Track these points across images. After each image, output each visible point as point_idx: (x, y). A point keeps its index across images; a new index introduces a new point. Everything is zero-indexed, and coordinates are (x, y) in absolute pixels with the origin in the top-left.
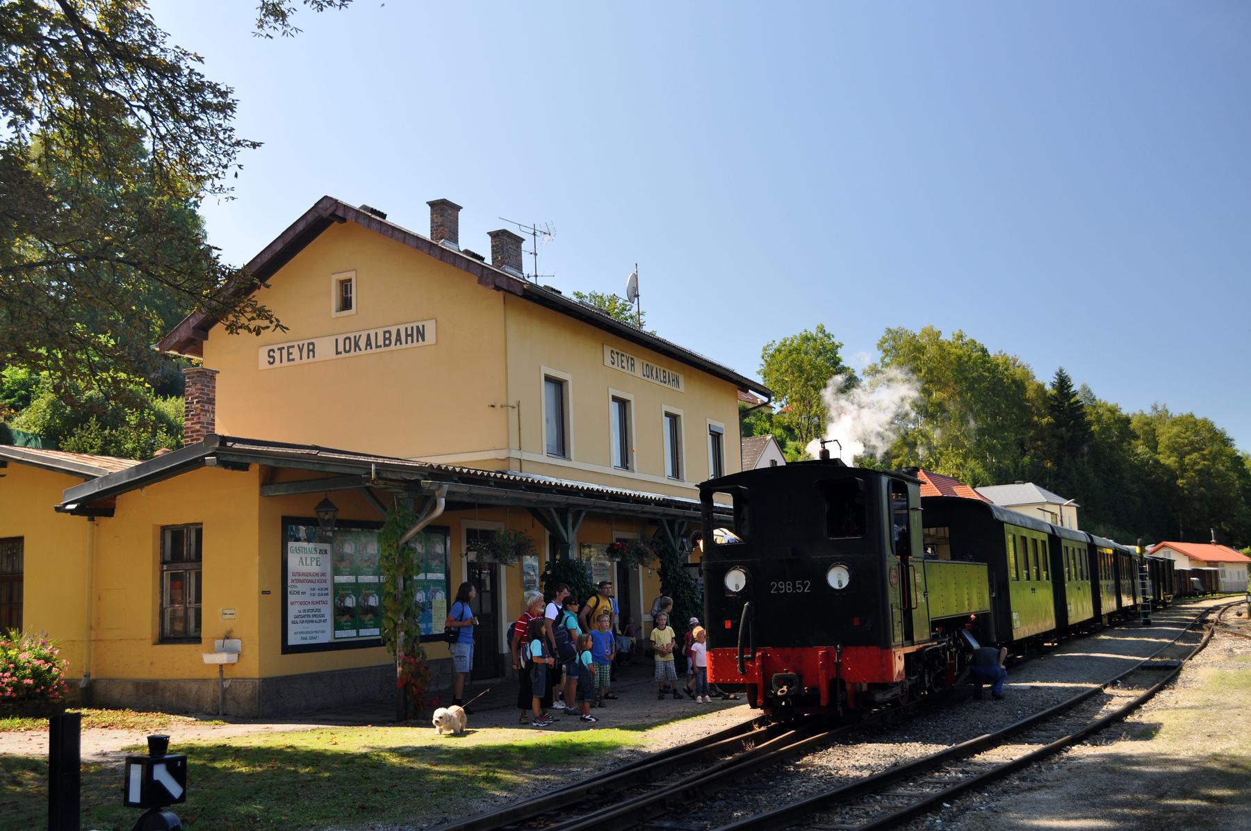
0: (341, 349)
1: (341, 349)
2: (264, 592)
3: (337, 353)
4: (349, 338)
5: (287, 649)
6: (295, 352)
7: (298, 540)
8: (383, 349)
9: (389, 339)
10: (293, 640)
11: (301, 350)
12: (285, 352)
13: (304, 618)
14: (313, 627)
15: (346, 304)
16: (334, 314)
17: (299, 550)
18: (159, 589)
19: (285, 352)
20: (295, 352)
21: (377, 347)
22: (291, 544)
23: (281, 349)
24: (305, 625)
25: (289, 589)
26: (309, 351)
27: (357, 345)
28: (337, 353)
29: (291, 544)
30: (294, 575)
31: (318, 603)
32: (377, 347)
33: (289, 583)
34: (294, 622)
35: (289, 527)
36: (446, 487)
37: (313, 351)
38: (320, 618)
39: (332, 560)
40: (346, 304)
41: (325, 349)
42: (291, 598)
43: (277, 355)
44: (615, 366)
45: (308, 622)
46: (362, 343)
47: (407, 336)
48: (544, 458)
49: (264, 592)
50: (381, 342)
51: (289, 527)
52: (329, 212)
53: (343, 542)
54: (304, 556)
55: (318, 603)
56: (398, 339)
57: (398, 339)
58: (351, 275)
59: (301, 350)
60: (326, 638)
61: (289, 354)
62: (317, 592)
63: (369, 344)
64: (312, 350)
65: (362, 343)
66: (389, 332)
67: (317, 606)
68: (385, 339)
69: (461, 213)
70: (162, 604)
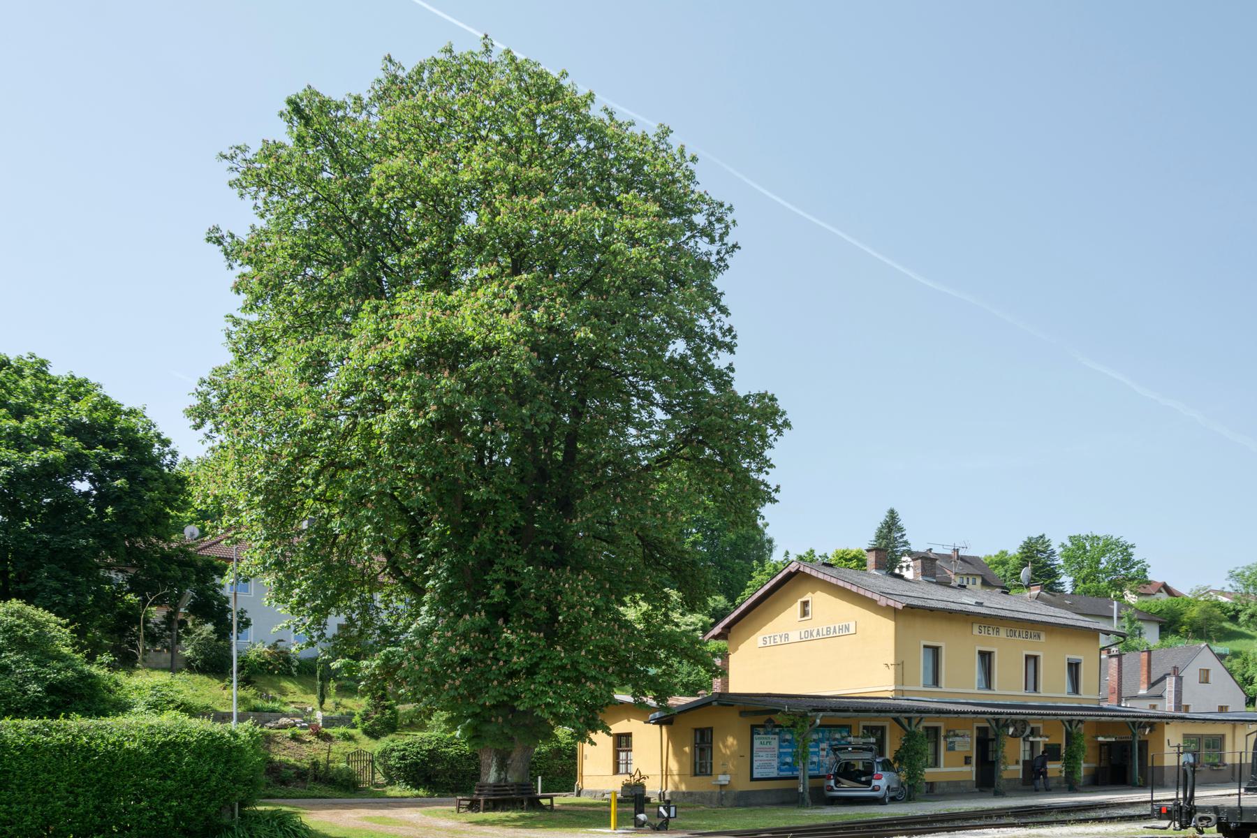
5: (752, 779)
36: (821, 714)
40: (805, 613)
60: (775, 775)
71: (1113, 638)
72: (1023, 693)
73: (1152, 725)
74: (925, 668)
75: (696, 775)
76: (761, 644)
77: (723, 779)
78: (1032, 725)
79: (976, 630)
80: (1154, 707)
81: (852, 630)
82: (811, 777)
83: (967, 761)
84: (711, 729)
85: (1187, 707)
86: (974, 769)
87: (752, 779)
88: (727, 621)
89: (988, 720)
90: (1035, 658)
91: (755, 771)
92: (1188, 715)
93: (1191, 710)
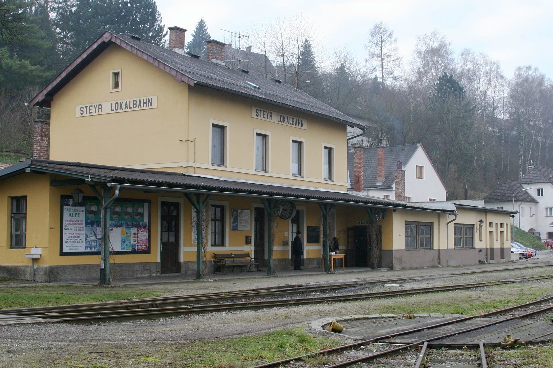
0: (114, 108)
1: (114, 108)
2: (51, 228)
3: (112, 110)
4: (117, 103)
5: (62, 254)
6: (93, 108)
7: (68, 205)
8: (133, 109)
9: (136, 104)
10: (65, 250)
11: (95, 108)
12: (88, 108)
13: (71, 240)
14: (75, 244)
15: (117, 85)
16: (111, 91)
17: (69, 210)
18: (10, 225)
19: (88, 108)
20: (93, 108)
21: (130, 108)
22: (65, 207)
23: (86, 107)
24: (72, 243)
25: (64, 227)
26: (99, 108)
27: (121, 106)
28: (112, 110)
29: (65, 207)
30: (66, 221)
31: (78, 234)
32: (130, 108)
33: (64, 224)
34: (66, 242)
35: (64, 200)
36: (119, 185)
37: (101, 108)
38: (80, 241)
39: (86, 214)
40: (117, 85)
41: (107, 108)
42: (64, 231)
43: (84, 110)
44: (259, 117)
45: (74, 242)
46: (123, 106)
47: (144, 103)
48: (210, 166)
49: (51, 228)
50: (132, 106)
51: (64, 200)
52: (108, 39)
53: (91, 206)
54: (71, 213)
55: (78, 234)
56: (140, 105)
57: (140, 105)
58: (120, 71)
59: (95, 108)
60: (82, 250)
61: (90, 110)
62: (78, 229)
63: (126, 107)
64: (100, 108)
65: (123, 106)
66: (136, 101)
67: (78, 235)
68: (134, 104)
69: (186, 33)
70: (11, 232)
71: (358, 131)
72: (210, 166)
73: (384, 211)
74: (257, 155)
75: (12, 247)
76: (78, 113)
77: (36, 252)
78: (298, 208)
79: (254, 114)
80: (502, 208)
81: (154, 105)
82: (466, 245)
83: (248, 241)
84: (25, 198)
85: (409, 198)
86: (253, 248)
87: (62, 254)
88: (50, 88)
89: (262, 199)
90: (223, 128)
91: (65, 245)
92: (408, 204)
93: (412, 200)
